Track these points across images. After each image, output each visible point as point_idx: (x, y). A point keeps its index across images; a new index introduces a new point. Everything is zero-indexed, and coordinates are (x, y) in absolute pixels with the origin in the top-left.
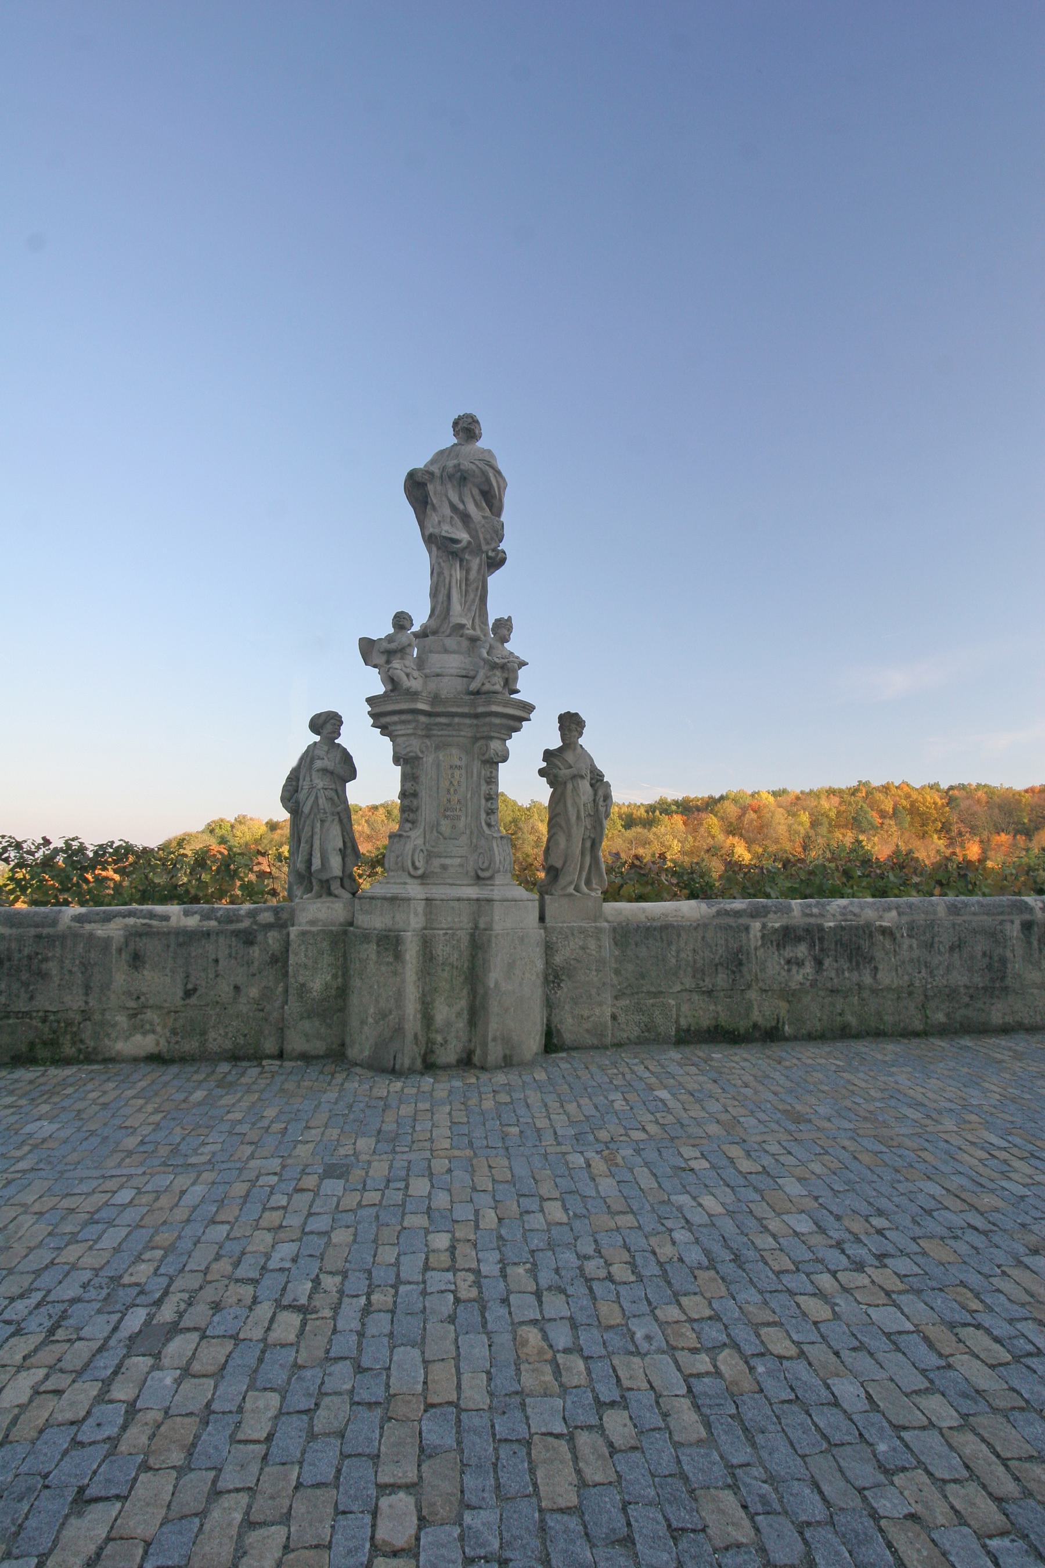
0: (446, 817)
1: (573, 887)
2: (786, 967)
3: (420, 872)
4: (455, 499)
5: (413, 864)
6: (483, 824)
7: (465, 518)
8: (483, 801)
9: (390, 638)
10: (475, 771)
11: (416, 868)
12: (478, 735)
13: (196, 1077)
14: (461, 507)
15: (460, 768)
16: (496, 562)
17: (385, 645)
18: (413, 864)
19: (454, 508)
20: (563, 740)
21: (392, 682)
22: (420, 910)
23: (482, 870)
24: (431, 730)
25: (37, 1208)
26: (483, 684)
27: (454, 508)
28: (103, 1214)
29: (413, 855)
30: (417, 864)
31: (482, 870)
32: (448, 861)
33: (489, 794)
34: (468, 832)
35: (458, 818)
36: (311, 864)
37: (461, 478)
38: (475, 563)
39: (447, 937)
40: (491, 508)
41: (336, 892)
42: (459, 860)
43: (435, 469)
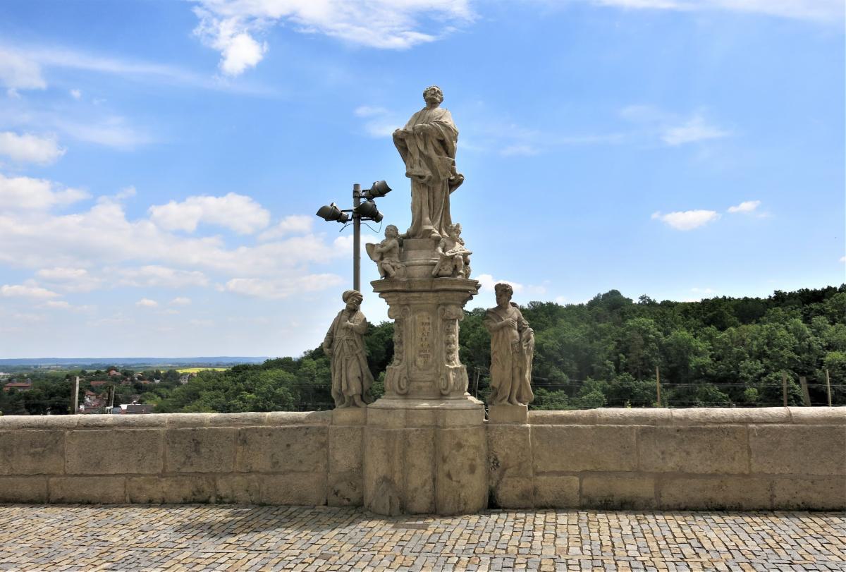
0: (420, 356)
1: (507, 399)
2: (661, 457)
3: (405, 391)
4: (422, 148)
5: (399, 386)
6: (444, 359)
7: (429, 160)
8: (444, 345)
9: (382, 245)
10: (439, 326)
11: (402, 389)
12: (440, 302)
13: (276, 513)
14: (426, 153)
15: (429, 324)
16: (455, 183)
17: (379, 249)
18: (399, 386)
19: (421, 154)
20: (498, 303)
21: (386, 274)
22: (402, 415)
23: (444, 390)
24: (409, 300)
25: (184, 562)
26: (440, 270)
27: (421, 154)
28: (212, 566)
29: (399, 382)
30: (402, 386)
31: (444, 390)
32: (422, 384)
33: (448, 340)
34: (435, 365)
35: (428, 356)
36: (341, 387)
37: (424, 135)
38: (439, 187)
39: (418, 432)
40: (447, 153)
41: (358, 404)
42: (429, 383)
43: (410, 129)
